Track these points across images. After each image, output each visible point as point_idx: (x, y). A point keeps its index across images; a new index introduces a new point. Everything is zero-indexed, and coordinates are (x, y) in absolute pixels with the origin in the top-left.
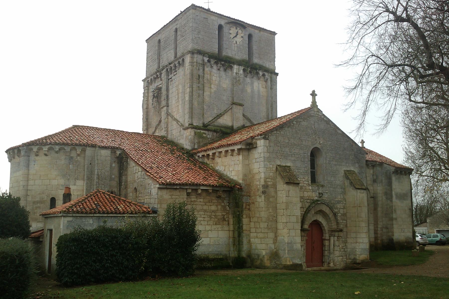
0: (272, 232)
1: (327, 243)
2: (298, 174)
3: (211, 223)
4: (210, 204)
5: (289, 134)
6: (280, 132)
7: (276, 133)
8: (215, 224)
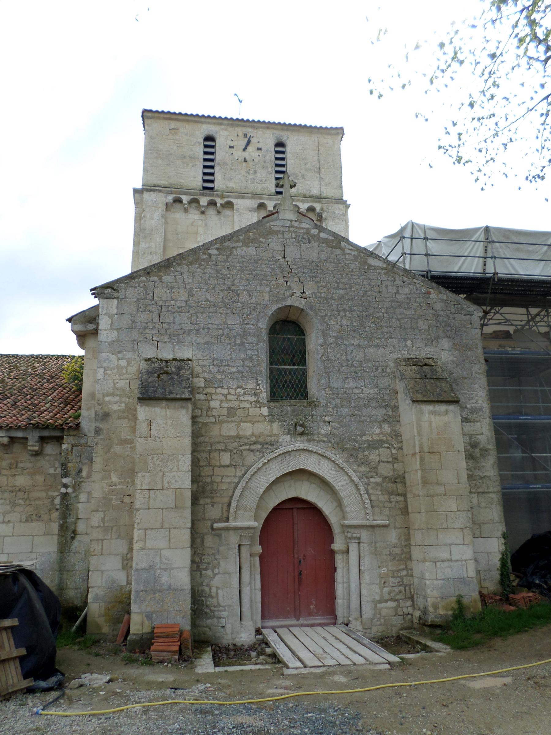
0: (119, 537)
1: (339, 560)
2: (219, 377)
3: (15, 516)
4: (13, 471)
5: (190, 281)
6: (160, 278)
7: (147, 281)
8: (27, 521)
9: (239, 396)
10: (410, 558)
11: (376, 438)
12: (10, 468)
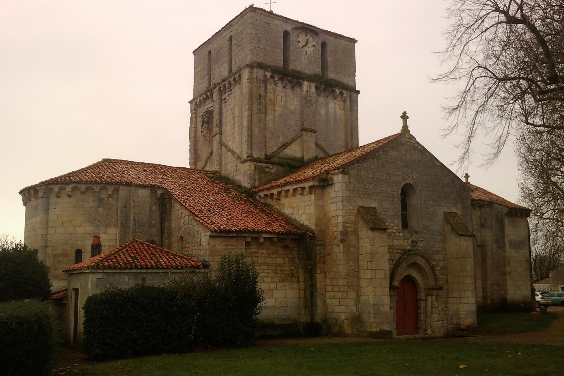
0: (353, 291)
1: (422, 304)
9: (392, 227)
10: (448, 303)
11: (438, 249)
12: (274, 254)
